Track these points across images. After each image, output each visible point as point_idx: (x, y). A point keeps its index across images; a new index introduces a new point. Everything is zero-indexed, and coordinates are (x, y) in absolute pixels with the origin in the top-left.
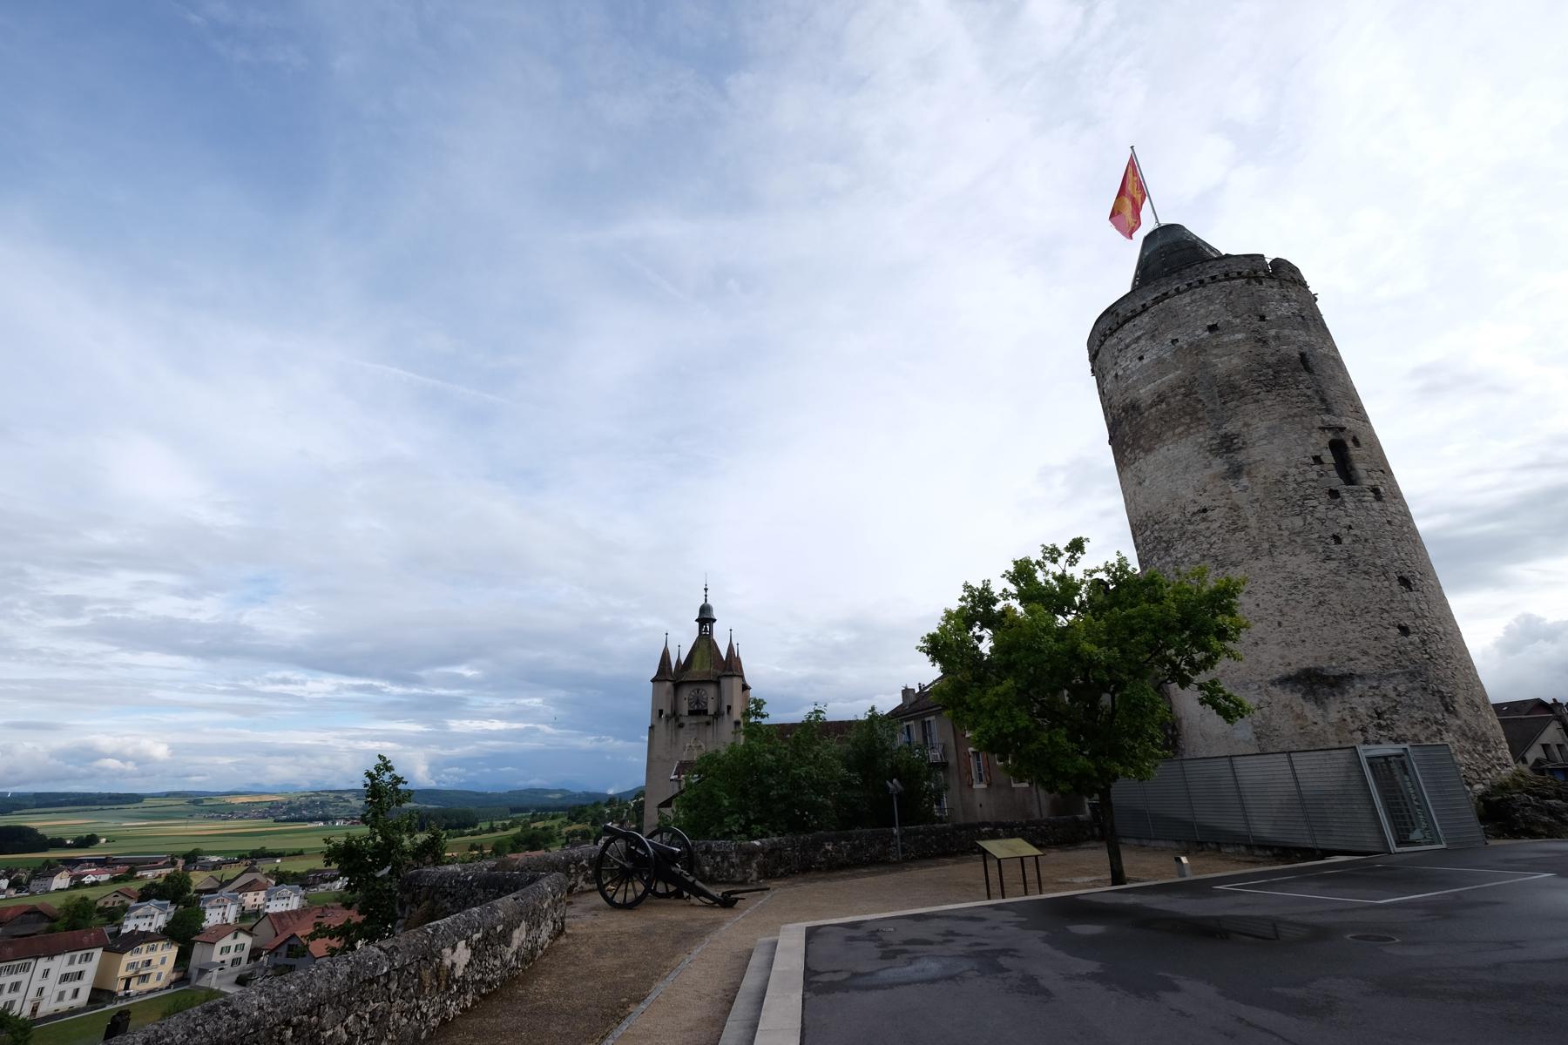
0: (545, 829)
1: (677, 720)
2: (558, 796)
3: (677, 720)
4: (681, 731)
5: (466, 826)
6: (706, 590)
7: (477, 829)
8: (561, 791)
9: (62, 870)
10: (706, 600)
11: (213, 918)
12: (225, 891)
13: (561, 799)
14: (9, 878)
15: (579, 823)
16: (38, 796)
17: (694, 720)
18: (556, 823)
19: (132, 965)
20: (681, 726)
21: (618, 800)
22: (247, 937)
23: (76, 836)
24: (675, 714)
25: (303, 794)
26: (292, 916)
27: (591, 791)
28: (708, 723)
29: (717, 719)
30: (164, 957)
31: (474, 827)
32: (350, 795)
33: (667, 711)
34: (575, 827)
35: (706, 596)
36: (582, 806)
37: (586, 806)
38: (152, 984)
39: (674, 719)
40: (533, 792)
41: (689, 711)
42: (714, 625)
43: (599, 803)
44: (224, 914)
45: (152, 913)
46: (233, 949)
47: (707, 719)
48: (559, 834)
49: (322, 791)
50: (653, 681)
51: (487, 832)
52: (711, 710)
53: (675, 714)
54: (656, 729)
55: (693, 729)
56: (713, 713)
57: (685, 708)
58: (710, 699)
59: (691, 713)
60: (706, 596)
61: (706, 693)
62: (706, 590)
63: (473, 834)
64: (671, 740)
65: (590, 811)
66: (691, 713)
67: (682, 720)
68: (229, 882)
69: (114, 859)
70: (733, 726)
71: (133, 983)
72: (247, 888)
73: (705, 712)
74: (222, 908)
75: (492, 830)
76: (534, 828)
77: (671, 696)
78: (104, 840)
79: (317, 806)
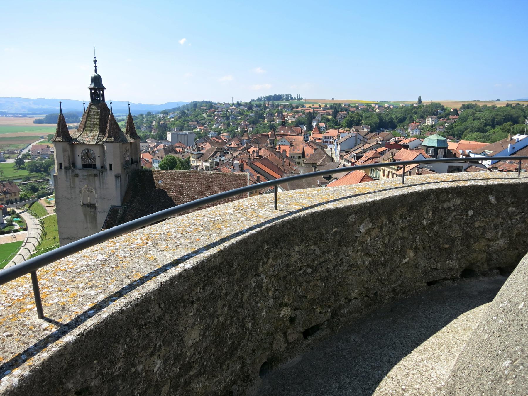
1: (73, 171)
4: (77, 179)
6: (95, 62)
10: (96, 71)
17: (85, 172)
20: (77, 175)
28: (96, 175)
29: (102, 173)
35: (96, 67)
42: (105, 91)
47: (95, 172)
55: (85, 179)
57: (79, 162)
59: (85, 166)
60: (96, 67)
61: (93, 153)
62: (95, 62)
64: (71, 185)
66: (85, 166)
67: (77, 171)
70: (113, 178)
73: (95, 166)
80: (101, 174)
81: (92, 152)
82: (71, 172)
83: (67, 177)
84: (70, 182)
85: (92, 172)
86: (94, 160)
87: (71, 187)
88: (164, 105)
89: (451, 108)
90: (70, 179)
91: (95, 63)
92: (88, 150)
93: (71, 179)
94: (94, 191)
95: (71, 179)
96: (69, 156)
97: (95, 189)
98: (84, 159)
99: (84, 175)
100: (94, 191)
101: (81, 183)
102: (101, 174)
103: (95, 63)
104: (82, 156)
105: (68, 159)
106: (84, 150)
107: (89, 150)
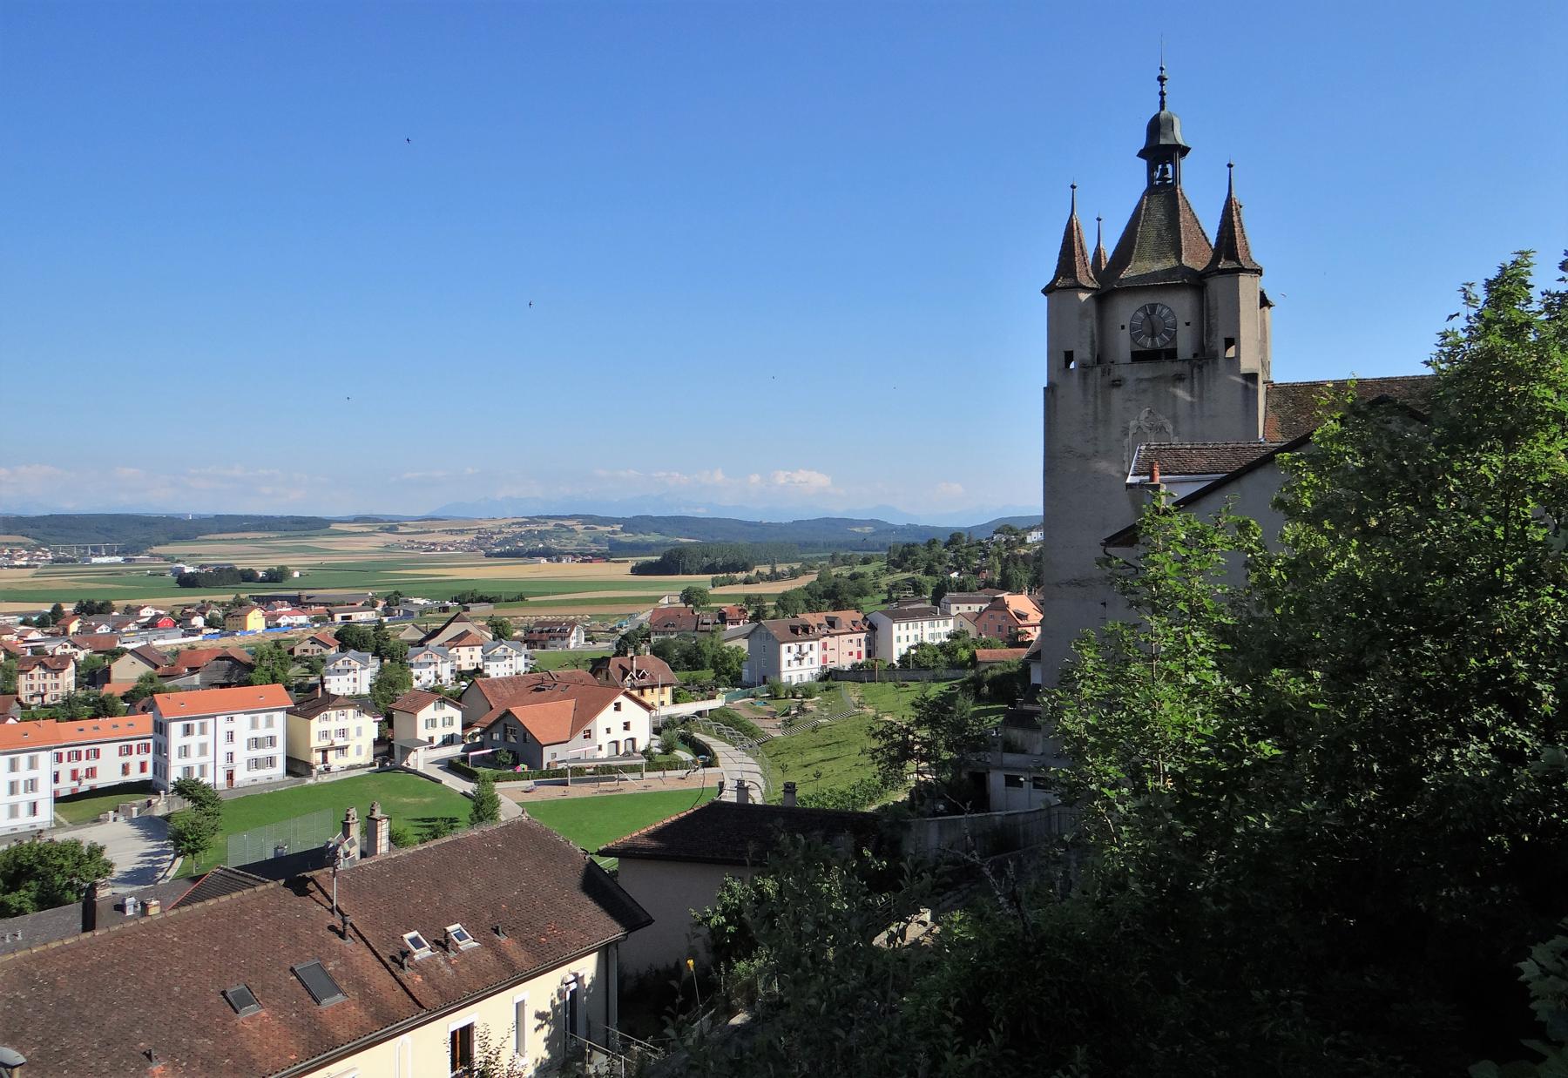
0: (854, 577)
1: (1106, 372)
2: (868, 529)
3: (1106, 372)
4: (1117, 396)
5: (736, 568)
6: (1161, 79)
7: (753, 573)
8: (872, 522)
9: (254, 608)
11: (423, 676)
12: (433, 643)
13: (873, 534)
14: (203, 614)
15: (904, 571)
16: (219, 518)
17: (1146, 370)
18: (869, 569)
19: (325, 734)
20: (1117, 383)
21: (965, 538)
22: (456, 710)
23: (266, 568)
24: (1101, 358)
25: (515, 520)
26: (507, 685)
27: (920, 524)
29: (1200, 367)
30: (365, 729)
31: (747, 571)
32: (575, 523)
33: (1084, 353)
34: (900, 576)
35: (1162, 94)
36: (908, 545)
37: (914, 545)
38: (352, 758)
39: (1099, 370)
40: (829, 522)
41: (1133, 353)
43: (934, 541)
44: (436, 672)
45: (352, 666)
46: (439, 723)
47: (1176, 368)
48: (876, 586)
49: (538, 517)
50: (1046, 291)
51: (769, 579)
52: (1185, 344)
53: (1101, 358)
54: (1060, 392)
55: (1144, 391)
56: (1190, 356)
57: (1123, 345)
58: (1181, 326)
59: (1138, 357)
60: (1162, 94)
62: (1161, 79)
63: (747, 582)
64: (1095, 413)
65: (922, 554)
66: (1138, 357)
67: (1118, 372)
68: (436, 633)
69: (308, 598)
71: (331, 755)
72: (459, 640)
73: (1171, 354)
74: (433, 666)
75: (775, 577)
76: (51, 841)
77: (1091, 323)
78: (296, 574)
79: (534, 536)
80: (1196, 371)
81: (1165, 311)
82: (1099, 375)
83: (1085, 392)
84: (1096, 408)
85: (1169, 368)
86: (1174, 338)
87: (1096, 419)
88: (781, 528)
89: (134, 608)
90: (1096, 397)
91: (1162, 85)
92: (1153, 307)
93: (1099, 396)
94: (1170, 428)
95: (1099, 396)
96: (1092, 331)
97: (1175, 420)
98: (1139, 335)
99: (1140, 380)
100: (1170, 428)
101: (1129, 404)
102: (1196, 371)
103: (1162, 85)
104: (1132, 328)
105: (1088, 340)
106: (1143, 309)
107: (1159, 308)
